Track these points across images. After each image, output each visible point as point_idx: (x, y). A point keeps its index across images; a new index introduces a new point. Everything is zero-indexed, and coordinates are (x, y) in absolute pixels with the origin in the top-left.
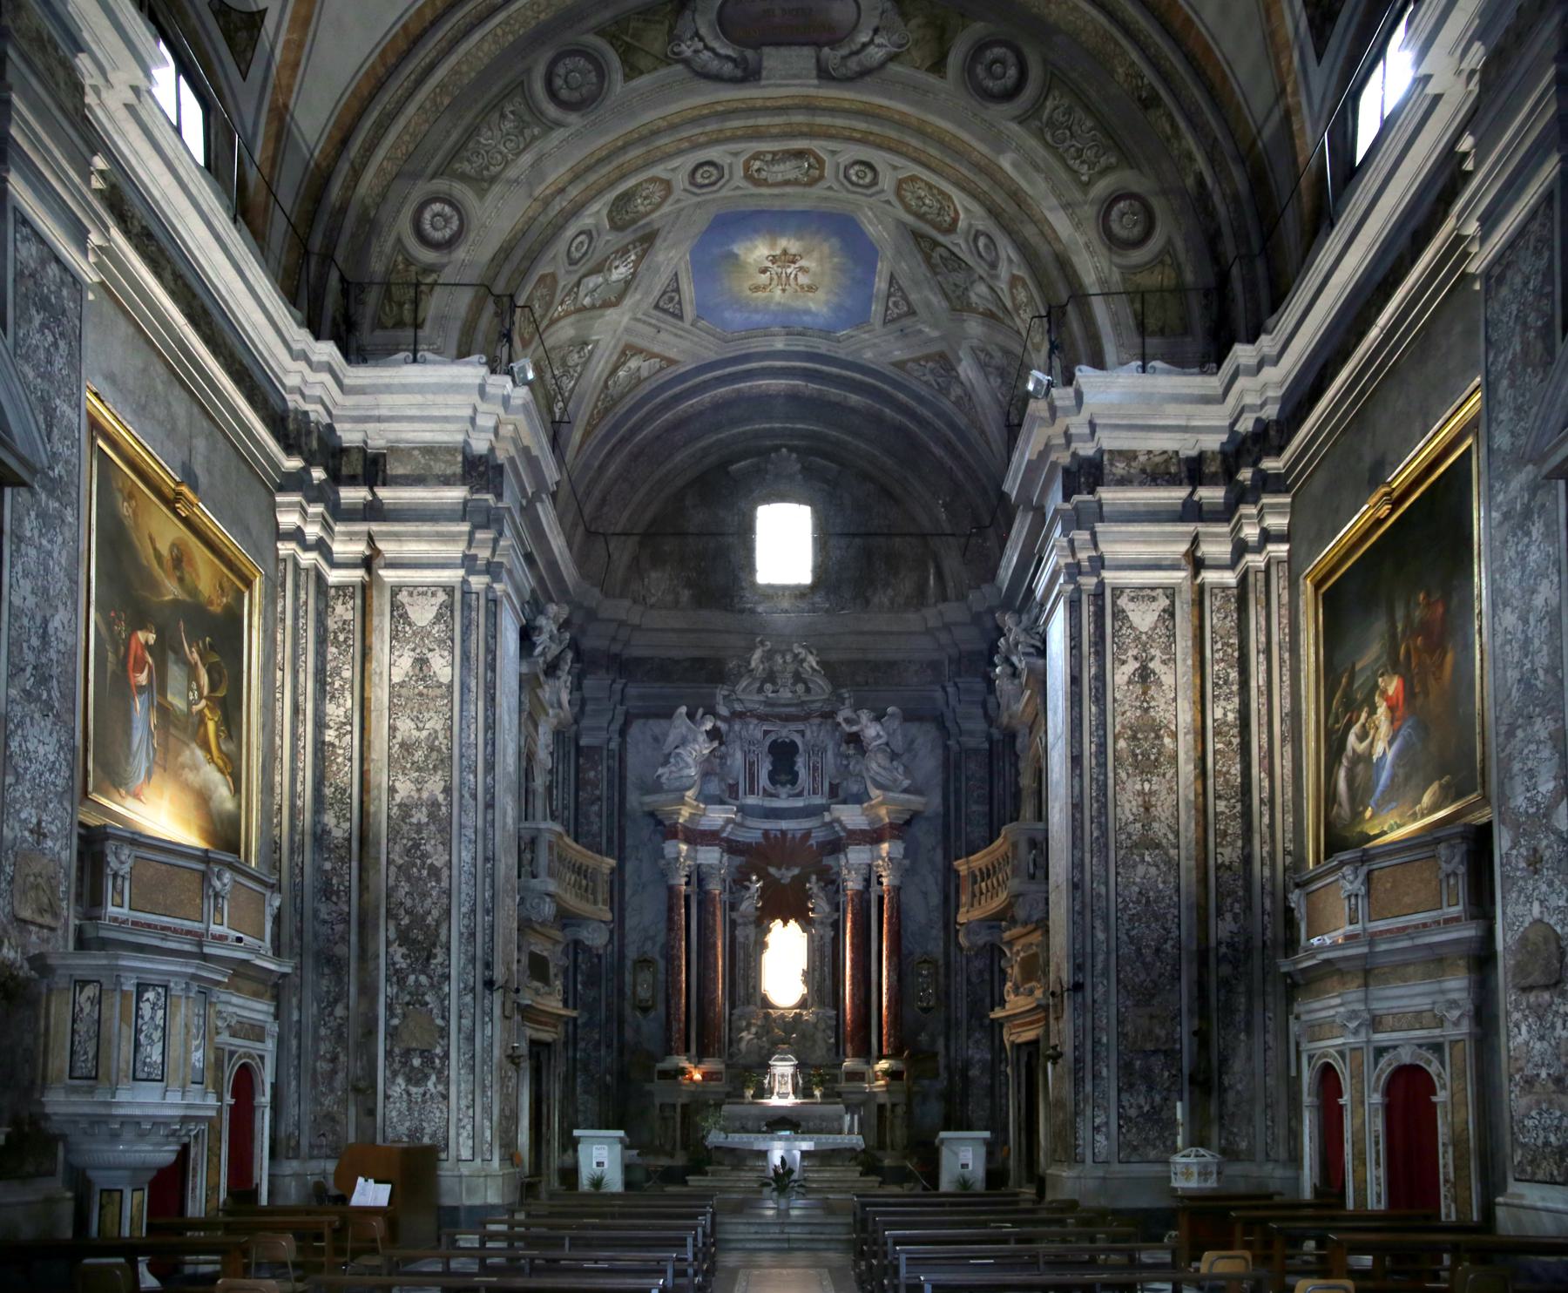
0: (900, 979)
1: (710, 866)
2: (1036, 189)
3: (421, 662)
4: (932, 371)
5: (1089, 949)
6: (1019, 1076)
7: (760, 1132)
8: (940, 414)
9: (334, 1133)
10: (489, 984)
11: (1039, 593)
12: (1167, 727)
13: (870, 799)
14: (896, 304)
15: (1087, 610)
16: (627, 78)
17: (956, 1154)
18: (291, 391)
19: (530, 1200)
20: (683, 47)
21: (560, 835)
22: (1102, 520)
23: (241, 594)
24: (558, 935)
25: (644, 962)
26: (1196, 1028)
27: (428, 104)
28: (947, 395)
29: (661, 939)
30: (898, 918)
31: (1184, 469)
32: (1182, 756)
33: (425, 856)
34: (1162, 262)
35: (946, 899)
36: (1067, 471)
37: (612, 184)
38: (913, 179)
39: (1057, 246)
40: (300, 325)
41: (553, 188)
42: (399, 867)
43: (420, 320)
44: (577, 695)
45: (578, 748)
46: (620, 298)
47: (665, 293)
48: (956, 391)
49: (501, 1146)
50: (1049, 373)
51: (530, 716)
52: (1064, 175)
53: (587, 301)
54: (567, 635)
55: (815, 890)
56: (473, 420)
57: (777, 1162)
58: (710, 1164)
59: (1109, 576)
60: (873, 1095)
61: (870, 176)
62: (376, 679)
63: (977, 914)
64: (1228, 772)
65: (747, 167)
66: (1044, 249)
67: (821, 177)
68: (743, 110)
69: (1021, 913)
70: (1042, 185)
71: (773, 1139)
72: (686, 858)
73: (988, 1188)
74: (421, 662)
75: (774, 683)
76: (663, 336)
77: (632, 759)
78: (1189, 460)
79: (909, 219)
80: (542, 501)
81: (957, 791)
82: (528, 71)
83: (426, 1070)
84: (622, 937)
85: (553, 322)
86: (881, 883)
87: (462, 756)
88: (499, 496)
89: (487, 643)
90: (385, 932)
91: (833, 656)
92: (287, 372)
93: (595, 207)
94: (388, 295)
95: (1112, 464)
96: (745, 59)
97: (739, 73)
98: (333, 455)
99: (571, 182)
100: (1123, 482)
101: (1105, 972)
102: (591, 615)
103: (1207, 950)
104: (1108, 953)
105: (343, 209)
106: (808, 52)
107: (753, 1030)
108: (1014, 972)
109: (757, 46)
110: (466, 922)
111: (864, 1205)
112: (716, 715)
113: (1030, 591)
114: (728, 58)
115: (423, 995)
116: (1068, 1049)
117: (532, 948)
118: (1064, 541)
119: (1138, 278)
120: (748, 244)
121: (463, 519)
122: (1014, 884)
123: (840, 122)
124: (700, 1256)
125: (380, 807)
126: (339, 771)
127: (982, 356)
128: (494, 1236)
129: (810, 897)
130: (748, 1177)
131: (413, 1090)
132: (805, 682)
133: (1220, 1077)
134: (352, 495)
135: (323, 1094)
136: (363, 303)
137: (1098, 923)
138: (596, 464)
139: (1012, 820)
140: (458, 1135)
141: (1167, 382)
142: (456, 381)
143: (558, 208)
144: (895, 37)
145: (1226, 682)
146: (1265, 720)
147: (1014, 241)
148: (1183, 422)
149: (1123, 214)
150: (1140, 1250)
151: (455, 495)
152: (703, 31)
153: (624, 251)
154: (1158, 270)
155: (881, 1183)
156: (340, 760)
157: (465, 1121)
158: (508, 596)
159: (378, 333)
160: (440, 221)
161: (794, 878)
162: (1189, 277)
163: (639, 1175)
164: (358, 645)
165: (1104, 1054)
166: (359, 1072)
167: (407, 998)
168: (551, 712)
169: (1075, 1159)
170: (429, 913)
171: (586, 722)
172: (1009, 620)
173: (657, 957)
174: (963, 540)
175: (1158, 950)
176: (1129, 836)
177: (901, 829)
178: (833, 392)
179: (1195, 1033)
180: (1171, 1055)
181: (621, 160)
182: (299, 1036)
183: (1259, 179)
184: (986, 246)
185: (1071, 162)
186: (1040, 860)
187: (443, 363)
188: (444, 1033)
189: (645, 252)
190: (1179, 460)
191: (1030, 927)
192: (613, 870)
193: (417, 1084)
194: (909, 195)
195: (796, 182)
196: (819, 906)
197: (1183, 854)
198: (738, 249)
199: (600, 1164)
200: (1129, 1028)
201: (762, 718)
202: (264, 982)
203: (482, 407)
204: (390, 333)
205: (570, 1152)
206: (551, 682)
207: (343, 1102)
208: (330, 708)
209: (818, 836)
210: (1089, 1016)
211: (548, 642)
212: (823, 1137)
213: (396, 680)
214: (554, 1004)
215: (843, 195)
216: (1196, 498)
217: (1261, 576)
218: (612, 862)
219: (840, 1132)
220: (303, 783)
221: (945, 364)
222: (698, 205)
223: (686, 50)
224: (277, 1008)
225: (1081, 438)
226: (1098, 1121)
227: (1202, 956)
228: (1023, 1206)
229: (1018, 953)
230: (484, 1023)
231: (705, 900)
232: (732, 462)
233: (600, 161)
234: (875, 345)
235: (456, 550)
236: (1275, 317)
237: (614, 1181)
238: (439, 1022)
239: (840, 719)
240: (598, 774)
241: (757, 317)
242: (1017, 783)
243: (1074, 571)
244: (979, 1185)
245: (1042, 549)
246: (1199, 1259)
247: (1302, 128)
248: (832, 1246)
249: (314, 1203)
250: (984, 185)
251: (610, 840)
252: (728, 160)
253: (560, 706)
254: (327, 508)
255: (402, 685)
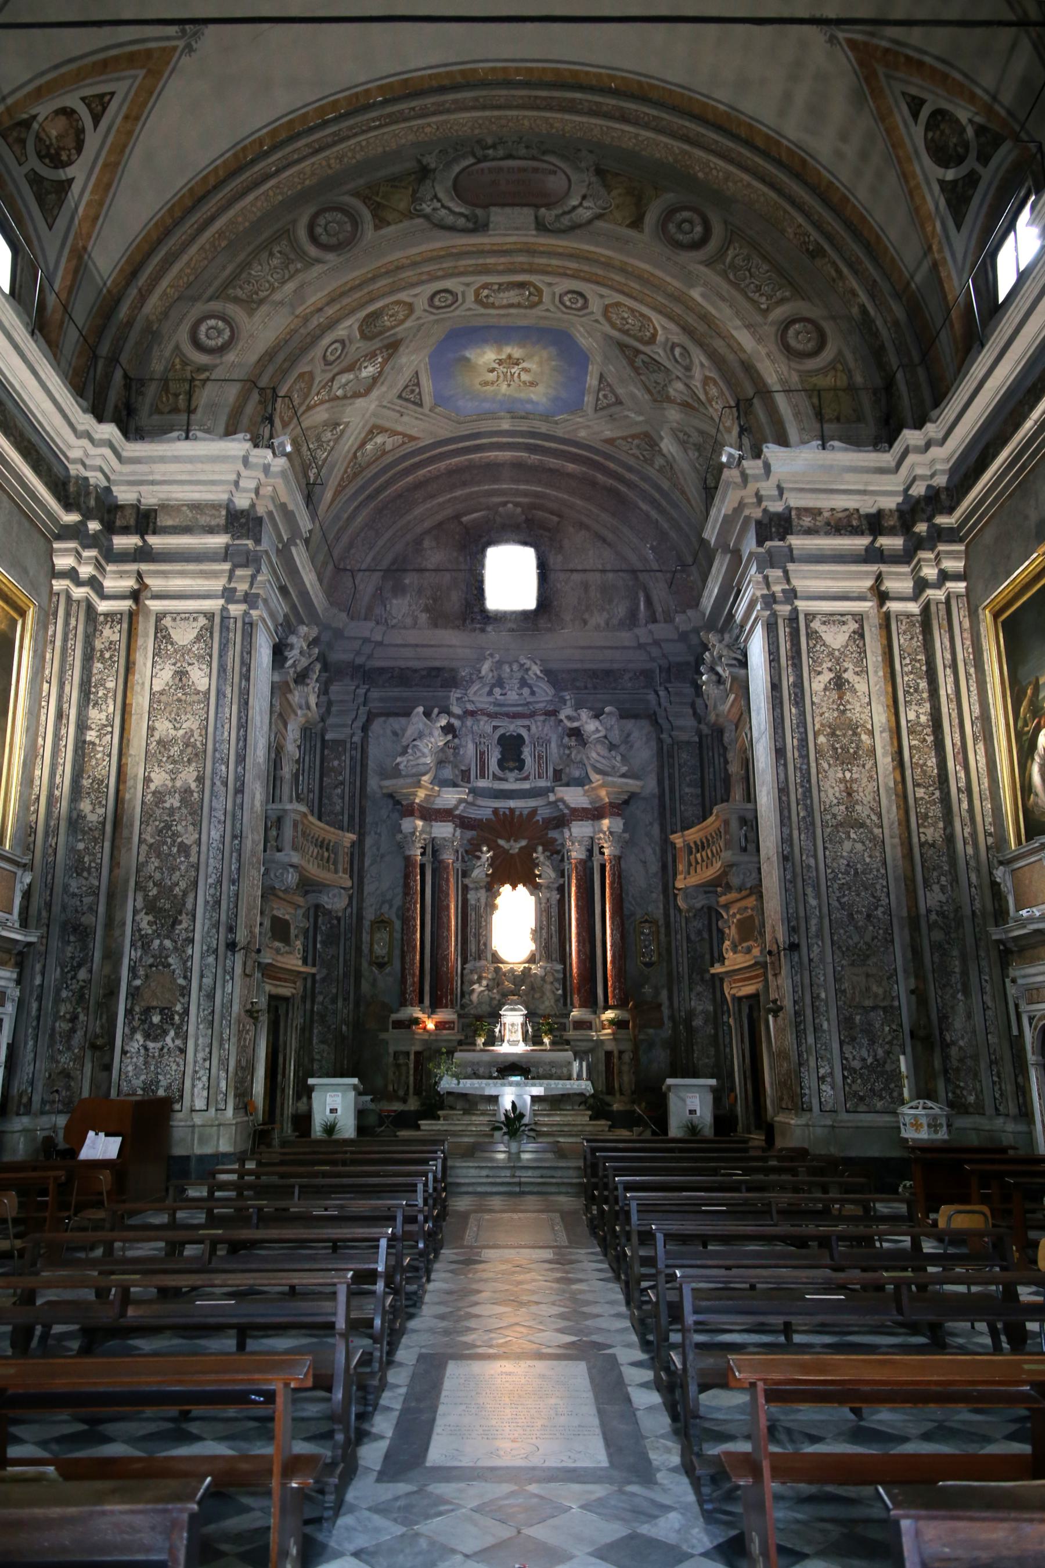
0: (623, 937)
1: (444, 839)
2: (723, 314)
3: (181, 674)
4: (638, 446)
5: (802, 914)
6: (741, 1027)
7: (491, 1077)
8: (646, 478)
9: (68, 1088)
10: (232, 946)
11: (739, 617)
12: (863, 726)
13: (591, 782)
14: (605, 396)
15: (783, 632)
16: (377, 228)
17: (684, 1100)
18: (74, 461)
19: (263, 1148)
20: (424, 206)
21: (305, 815)
22: (793, 560)
23: (15, 622)
24: (300, 900)
25: (381, 923)
26: (912, 987)
27: (207, 246)
28: (652, 465)
29: (398, 902)
30: (620, 883)
31: (864, 522)
32: (879, 751)
33: (176, 835)
34: (834, 368)
35: (664, 867)
36: (759, 523)
37: (362, 306)
38: (618, 304)
39: (742, 356)
40: (85, 411)
41: (312, 308)
42: (151, 846)
43: (193, 407)
44: (323, 698)
45: (323, 740)
46: (368, 391)
47: (407, 386)
48: (659, 461)
49: (235, 1096)
50: (740, 449)
51: (280, 716)
52: (748, 305)
53: (340, 393)
54: (316, 651)
55: (542, 858)
56: (236, 484)
57: (509, 1107)
58: (442, 1109)
59: (802, 605)
60: (600, 1043)
61: (581, 302)
62: (138, 688)
63: (693, 880)
64: (925, 764)
65: (477, 294)
66: (731, 357)
67: (540, 302)
68: (473, 253)
69: (735, 881)
70: (728, 311)
71: (504, 1085)
72: (422, 832)
73: (716, 1134)
74: (181, 674)
75: (502, 687)
76: (405, 419)
77: (373, 750)
78: (868, 516)
79: (615, 334)
80: (296, 545)
81: (671, 777)
82: (294, 222)
83: (165, 1027)
84: (361, 900)
85: (309, 408)
86: (603, 854)
87: (215, 750)
88: (258, 541)
89: (242, 657)
90: (132, 902)
91: (554, 666)
92: (70, 447)
93: (348, 323)
94: (166, 388)
95: (799, 518)
96: (476, 216)
97: (470, 225)
98: (109, 511)
99: (328, 304)
100: (810, 532)
101: (819, 934)
102: (338, 634)
103: (918, 916)
104: (821, 918)
105: (129, 324)
106: (527, 211)
107: (484, 983)
108: (732, 932)
109: (486, 207)
110: (212, 891)
111: (594, 1150)
112: (449, 713)
113: (731, 616)
114: (461, 214)
115: (167, 957)
116: (788, 1003)
117: (275, 912)
118: (759, 577)
119: (814, 380)
120: (479, 351)
121: (225, 560)
122: (727, 855)
123: (554, 262)
124: (430, 1202)
125: (135, 794)
126: (97, 764)
127: (681, 435)
128: (223, 1186)
129: (537, 865)
130: (478, 1122)
131: (151, 1045)
132: (530, 687)
133: (941, 1033)
134: (123, 542)
135: (60, 1052)
136: (142, 394)
137: (809, 891)
138: (346, 516)
139: (722, 801)
140: (193, 1086)
141: (842, 456)
142: (223, 453)
143: (316, 323)
144: (600, 202)
145: (916, 690)
146: (956, 722)
147: (705, 351)
148: (861, 487)
149: (798, 333)
150: (875, 1201)
151: (219, 541)
152: (441, 195)
153: (373, 355)
154: (831, 374)
155: (610, 1127)
156: (99, 756)
157: (201, 1073)
158: (264, 620)
159: (156, 417)
160: (213, 333)
161: (521, 848)
162: (859, 379)
163: (372, 1120)
164: (123, 661)
165: (823, 1009)
166: (98, 1030)
167: (151, 961)
168: (299, 712)
169: (802, 1108)
170: (177, 884)
171: (331, 720)
172: (712, 638)
173: (394, 918)
174: (669, 575)
175: (869, 916)
176: (834, 816)
177: (620, 807)
178: (553, 462)
179: (913, 992)
180: (891, 1012)
181: (371, 288)
182: (40, 999)
183: (915, 309)
184: (681, 354)
185: (751, 295)
186: (751, 835)
187: (213, 440)
188: (185, 992)
189: (390, 356)
190: (860, 516)
191: (744, 893)
192: (353, 844)
193: (155, 1040)
194: (614, 317)
195: (519, 306)
196: (546, 873)
197: (886, 831)
198: (468, 354)
199: (333, 1111)
200: (846, 985)
201: (492, 716)
202: (8, 951)
203: (244, 473)
204: (169, 417)
205: (305, 1099)
206: (300, 688)
207: (80, 1060)
208: (93, 713)
209: (544, 813)
210: (807, 974)
211: (298, 656)
212: (553, 1083)
213: (156, 688)
214: (293, 962)
215: (559, 315)
216: (877, 545)
217: (942, 607)
218: (353, 837)
219: (569, 1078)
220: (62, 776)
221: (650, 442)
222: (437, 321)
223: (427, 209)
224: (20, 974)
225: (771, 498)
226: (822, 1071)
227: (914, 922)
228: (752, 1153)
229: (734, 915)
230: (225, 981)
231: (439, 868)
232: (465, 514)
233: (352, 289)
234: (588, 427)
235: (218, 585)
236: (937, 411)
237: (347, 1128)
238: (181, 981)
239: (562, 716)
240: (341, 763)
241: (486, 406)
242: (726, 770)
243: (770, 600)
244: (708, 1132)
245: (740, 583)
246: (936, 1211)
247: (949, 276)
248: (563, 1189)
249: (41, 1158)
250: (678, 309)
251: (351, 817)
252: (462, 288)
253: (308, 708)
254: (100, 552)
255: (162, 693)
